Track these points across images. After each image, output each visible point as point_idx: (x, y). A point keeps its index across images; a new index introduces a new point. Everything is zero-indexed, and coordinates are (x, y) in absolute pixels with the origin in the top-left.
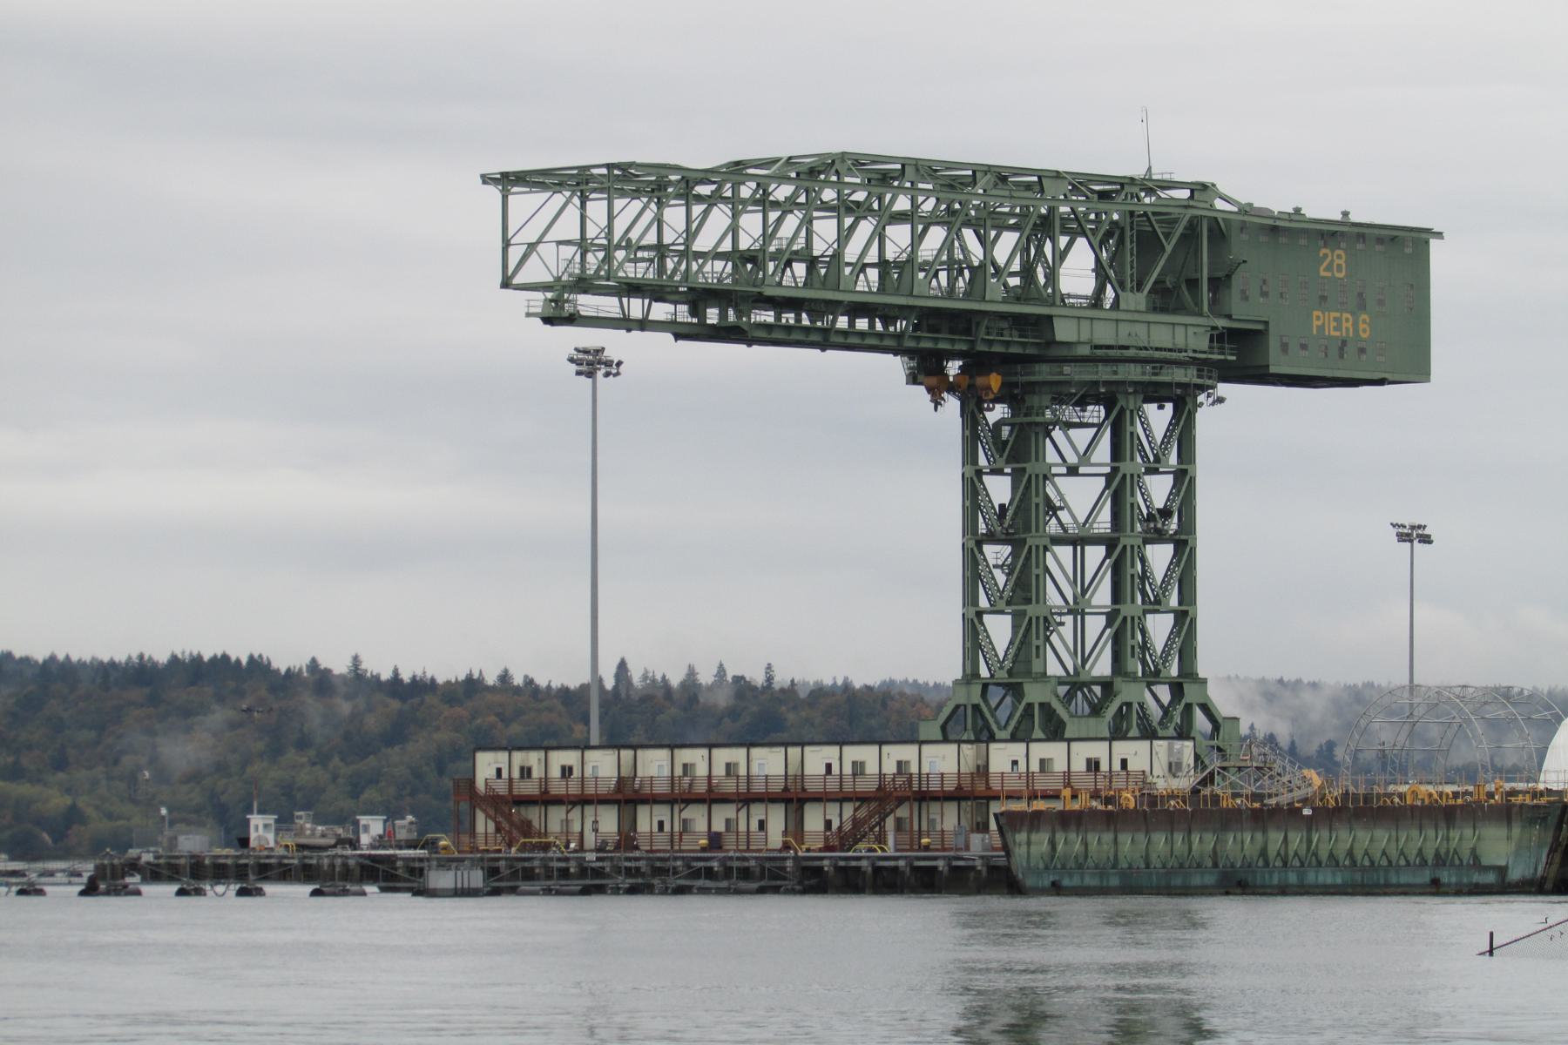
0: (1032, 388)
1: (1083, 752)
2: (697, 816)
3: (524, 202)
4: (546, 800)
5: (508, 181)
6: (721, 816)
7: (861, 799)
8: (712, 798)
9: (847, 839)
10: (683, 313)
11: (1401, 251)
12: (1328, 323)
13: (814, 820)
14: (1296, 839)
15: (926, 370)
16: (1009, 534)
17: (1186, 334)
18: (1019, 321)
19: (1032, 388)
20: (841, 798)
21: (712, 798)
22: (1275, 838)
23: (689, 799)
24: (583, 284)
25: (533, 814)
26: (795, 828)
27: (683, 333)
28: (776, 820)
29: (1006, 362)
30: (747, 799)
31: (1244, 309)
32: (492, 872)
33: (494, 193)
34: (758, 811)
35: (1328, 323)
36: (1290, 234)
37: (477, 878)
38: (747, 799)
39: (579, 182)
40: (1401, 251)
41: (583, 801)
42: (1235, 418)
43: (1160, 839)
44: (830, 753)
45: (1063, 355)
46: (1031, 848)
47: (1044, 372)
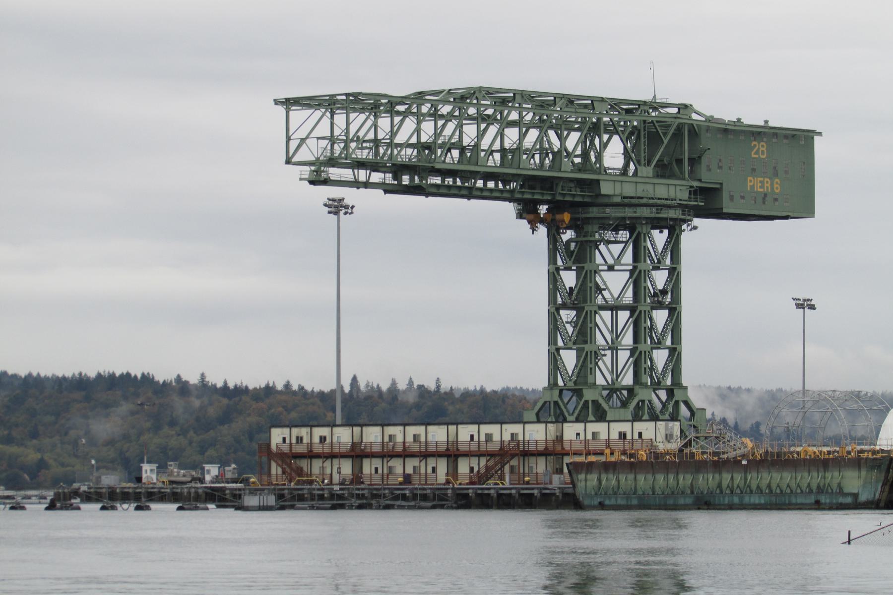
0: (588, 221)
1: (617, 428)
2: (397, 465)
3: (298, 115)
4: (311, 455)
5: (289, 103)
6: (411, 465)
7: (491, 455)
8: (406, 454)
9: (482, 478)
10: (389, 178)
11: (798, 143)
12: (757, 184)
13: (463, 467)
14: (738, 478)
15: (527, 211)
16: (575, 304)
17: (675, 190)
18: (580, 183)
19: (588, 221)
20: (479, 455)
21: (406, 454)
22: (726, 477)
23: (392, 455)
24: (332, 162)
25: (304, 464)
26: (453, 472)
27: (389, 190)
28: (442, 467)
29: (573, 206)
30: (425, 455)
31: (708, 176)
32: (280, 497)
33: (281, 110)
34: (431, 462)
35: (757, 184)
36: (734, 133)
37: (271, 500)
38: (425, 455)
39: (330, 104)
40: (798, 143)
41: (332, 456)
42: (703, 238)
43: (660, 478)
44: (473, 429)
45: (605, 202)
46: (587, 483)
47: (594, 212)
